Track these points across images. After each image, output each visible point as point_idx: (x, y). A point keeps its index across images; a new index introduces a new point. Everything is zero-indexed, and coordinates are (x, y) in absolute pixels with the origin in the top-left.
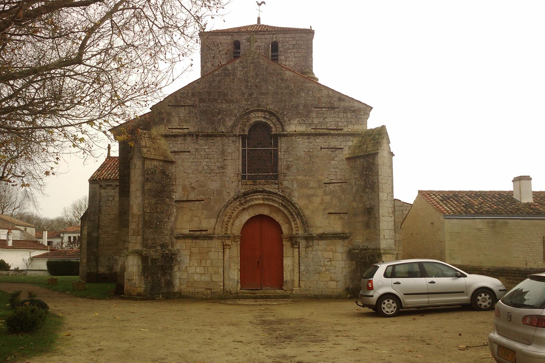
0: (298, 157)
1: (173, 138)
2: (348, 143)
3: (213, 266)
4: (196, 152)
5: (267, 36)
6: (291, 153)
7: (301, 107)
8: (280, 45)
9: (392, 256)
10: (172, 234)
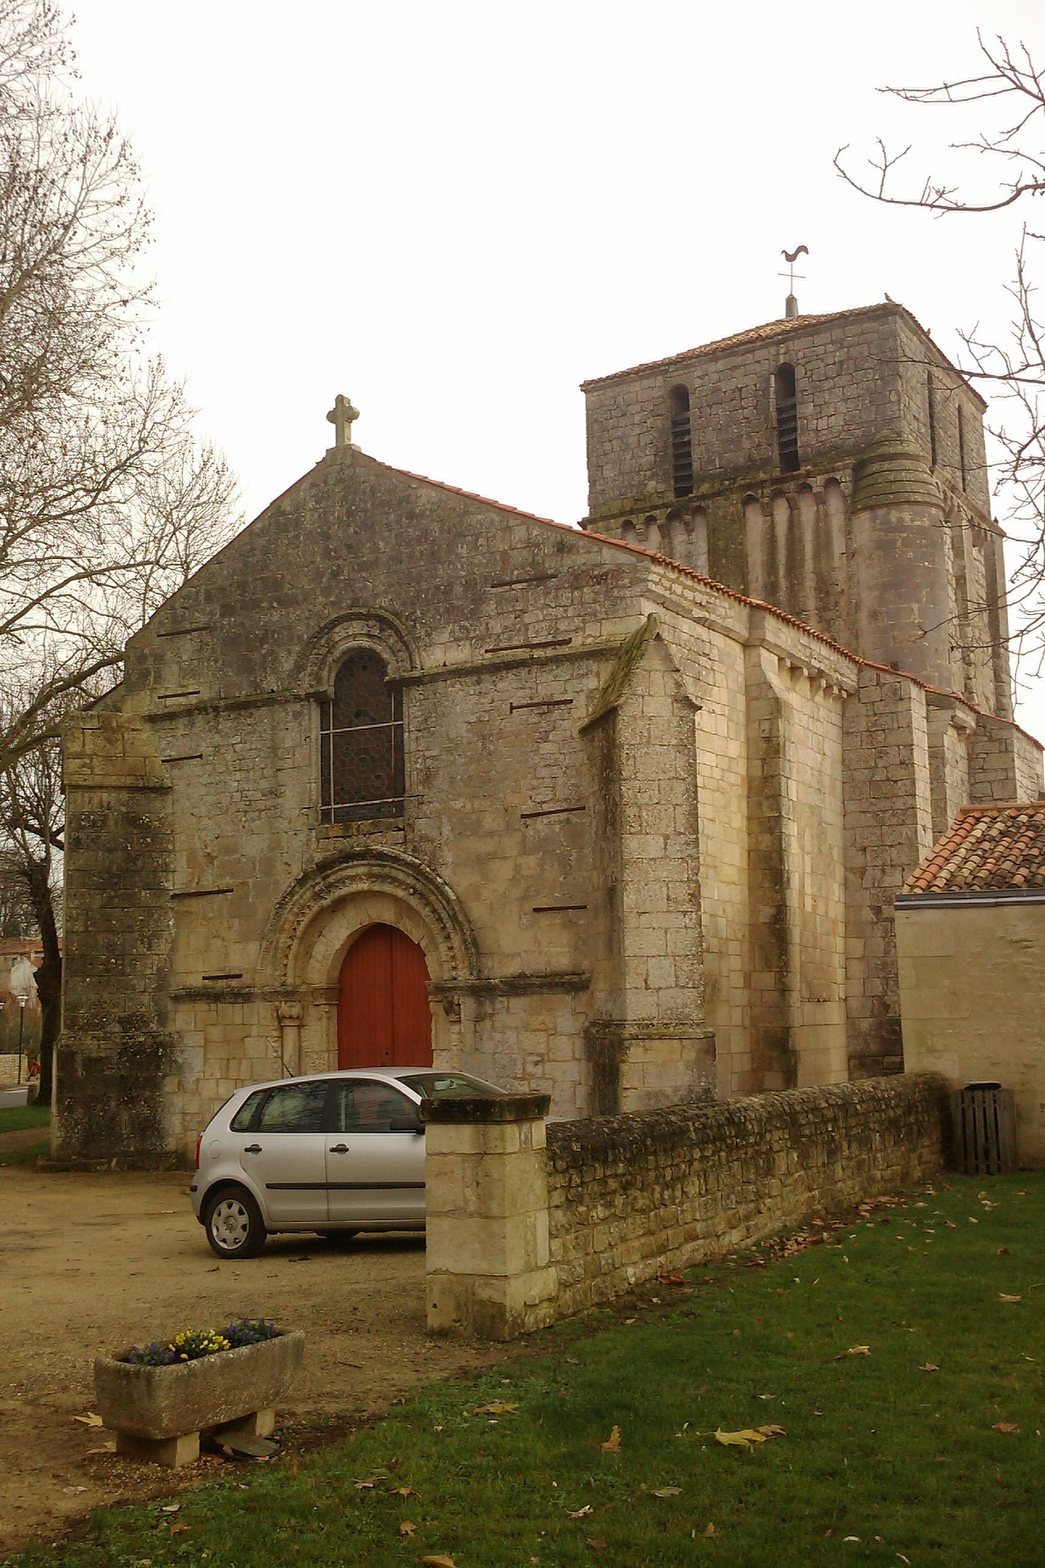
0: (451, 741)
1: (168, 722)
2: (584, 681)
4: (215, 755)
5: (760, 354)
6: (433, 733)
7: (458, 589)
8: (799, 372)
9: (683, 1047)
10: (159, 989)
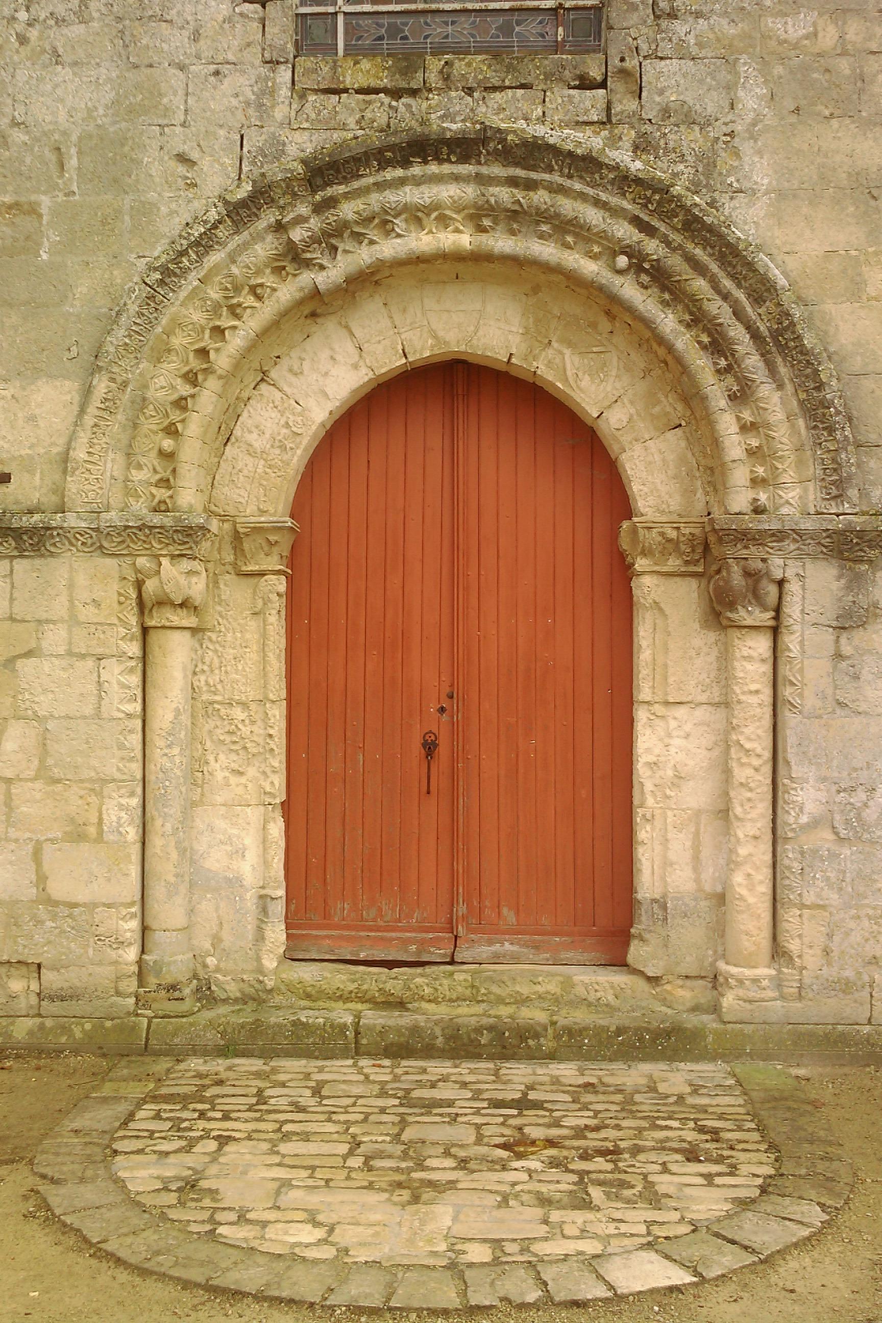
3: (57, 772)
